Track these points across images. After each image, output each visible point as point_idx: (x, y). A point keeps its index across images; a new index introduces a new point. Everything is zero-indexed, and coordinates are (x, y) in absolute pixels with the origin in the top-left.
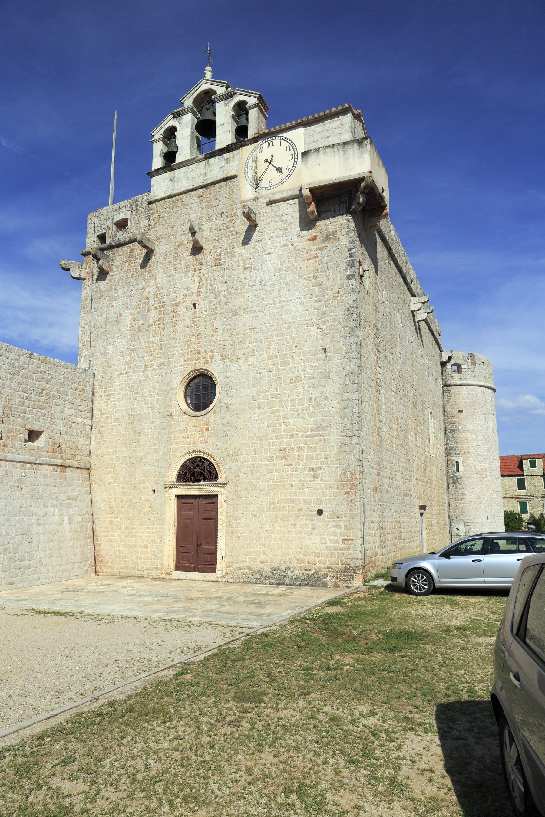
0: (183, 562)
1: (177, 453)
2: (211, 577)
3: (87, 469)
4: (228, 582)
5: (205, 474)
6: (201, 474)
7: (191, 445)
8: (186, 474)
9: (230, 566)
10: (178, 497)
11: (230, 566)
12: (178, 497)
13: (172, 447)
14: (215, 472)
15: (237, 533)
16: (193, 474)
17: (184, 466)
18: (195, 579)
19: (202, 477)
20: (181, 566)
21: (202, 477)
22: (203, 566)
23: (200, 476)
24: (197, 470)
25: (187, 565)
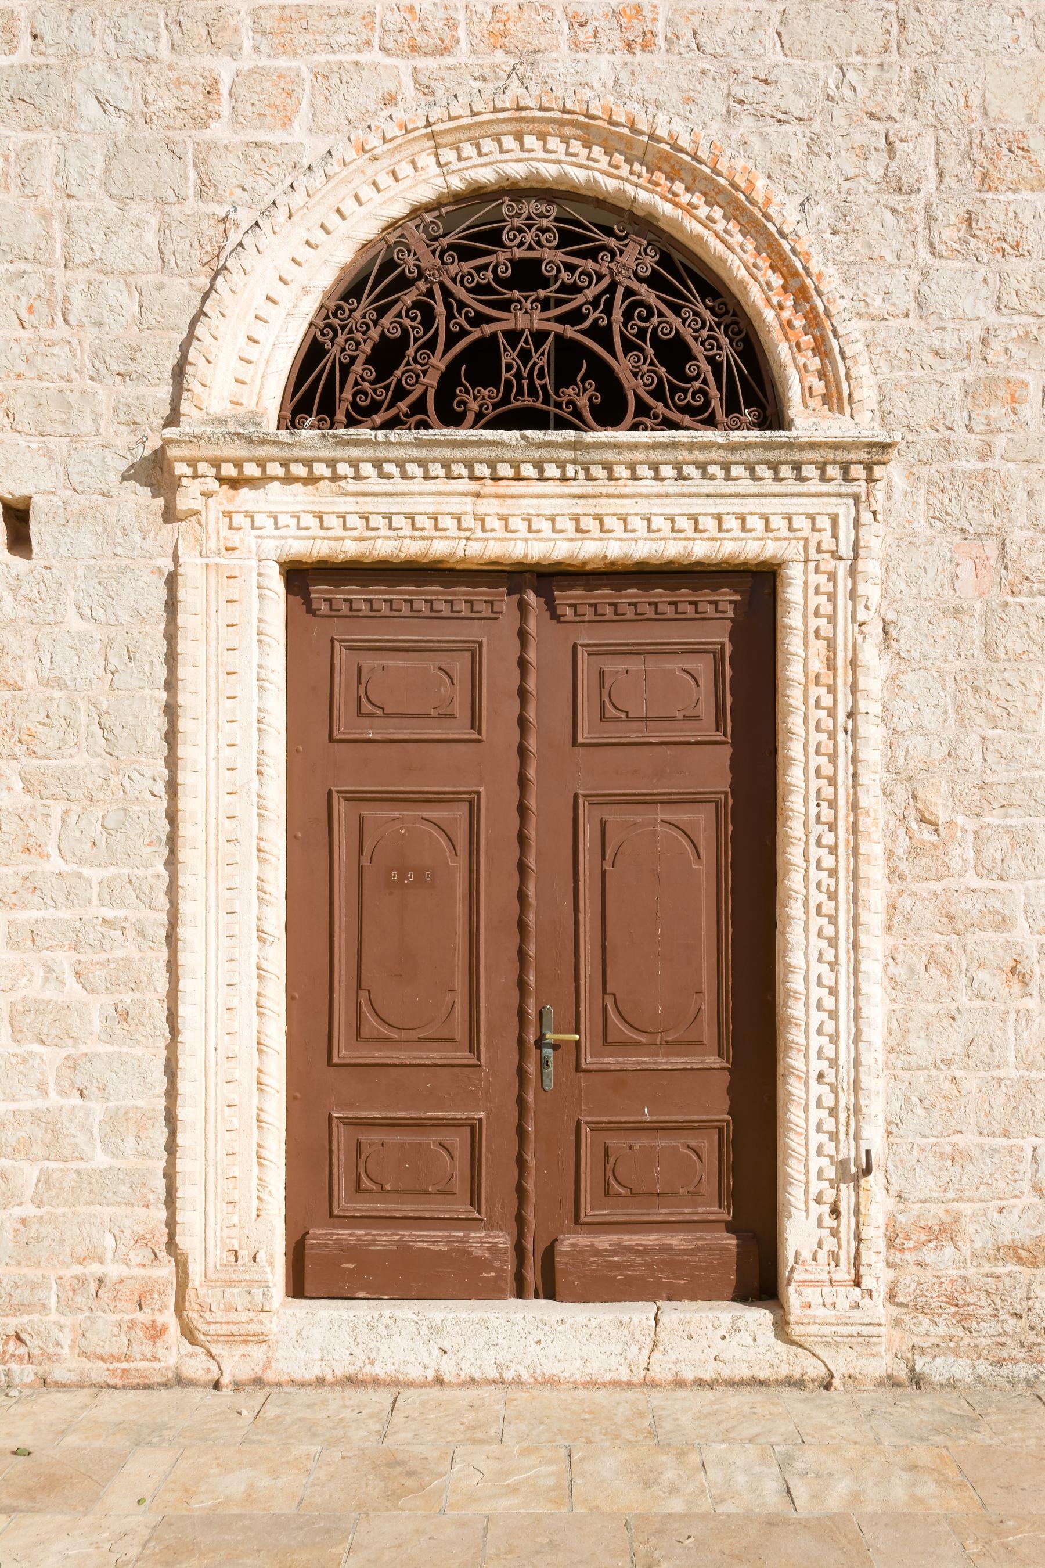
0: (363, 1207)
1: (298, 132)
2: (732, 1349)
3: (858, 1275)
4: (916, 1380)
5: (622, 366)
6: (569, 360)
7: (462, 55)
8: (387, 355)
9: (944, 1233)
10: (299, 577)
11: (944, 1233)
12: (299, 577)
13: (225, 70)
14: (363, 308)
15: (1002, 923)
16: (480, 363)
17: (378, 278)
18: (550, 1368)
19: (583, 395)
20: (353, 1252)
21: (583, 395)
22: (603, 1241)
23: (564, 377)
24: (528, 317)
25: (422, 1239)
